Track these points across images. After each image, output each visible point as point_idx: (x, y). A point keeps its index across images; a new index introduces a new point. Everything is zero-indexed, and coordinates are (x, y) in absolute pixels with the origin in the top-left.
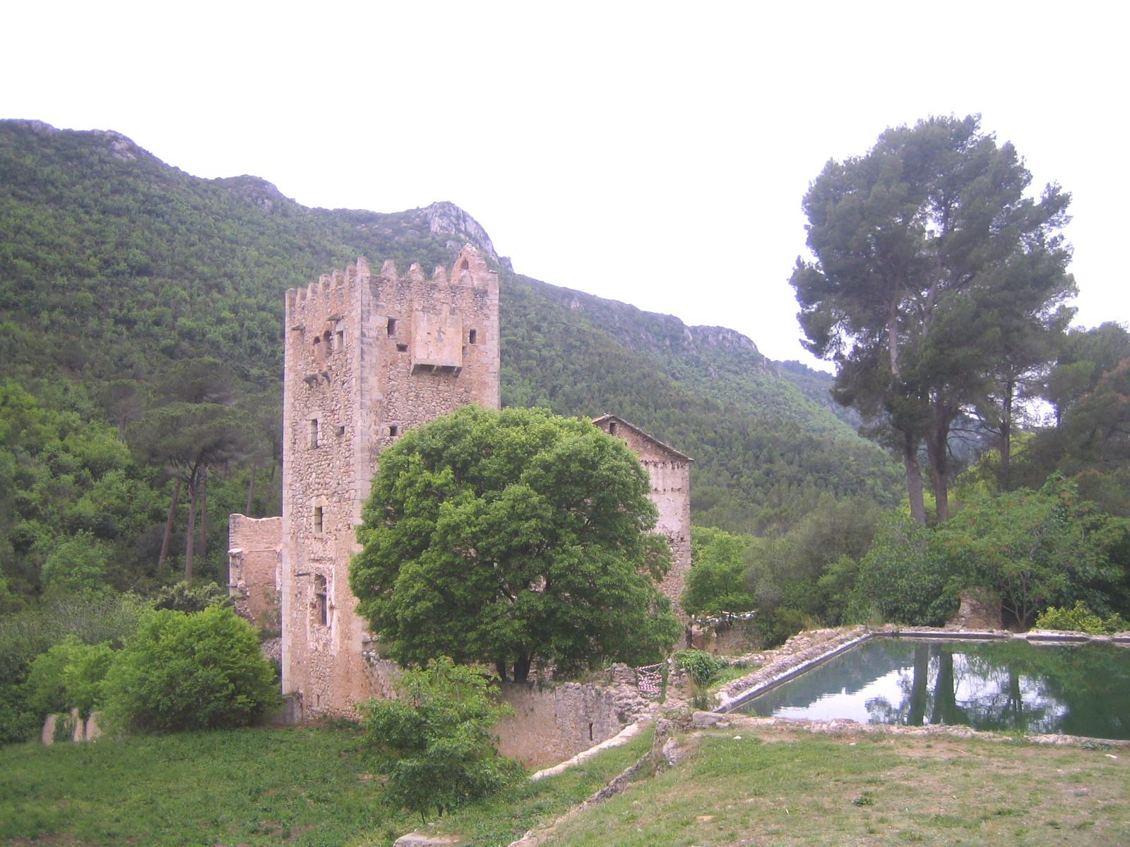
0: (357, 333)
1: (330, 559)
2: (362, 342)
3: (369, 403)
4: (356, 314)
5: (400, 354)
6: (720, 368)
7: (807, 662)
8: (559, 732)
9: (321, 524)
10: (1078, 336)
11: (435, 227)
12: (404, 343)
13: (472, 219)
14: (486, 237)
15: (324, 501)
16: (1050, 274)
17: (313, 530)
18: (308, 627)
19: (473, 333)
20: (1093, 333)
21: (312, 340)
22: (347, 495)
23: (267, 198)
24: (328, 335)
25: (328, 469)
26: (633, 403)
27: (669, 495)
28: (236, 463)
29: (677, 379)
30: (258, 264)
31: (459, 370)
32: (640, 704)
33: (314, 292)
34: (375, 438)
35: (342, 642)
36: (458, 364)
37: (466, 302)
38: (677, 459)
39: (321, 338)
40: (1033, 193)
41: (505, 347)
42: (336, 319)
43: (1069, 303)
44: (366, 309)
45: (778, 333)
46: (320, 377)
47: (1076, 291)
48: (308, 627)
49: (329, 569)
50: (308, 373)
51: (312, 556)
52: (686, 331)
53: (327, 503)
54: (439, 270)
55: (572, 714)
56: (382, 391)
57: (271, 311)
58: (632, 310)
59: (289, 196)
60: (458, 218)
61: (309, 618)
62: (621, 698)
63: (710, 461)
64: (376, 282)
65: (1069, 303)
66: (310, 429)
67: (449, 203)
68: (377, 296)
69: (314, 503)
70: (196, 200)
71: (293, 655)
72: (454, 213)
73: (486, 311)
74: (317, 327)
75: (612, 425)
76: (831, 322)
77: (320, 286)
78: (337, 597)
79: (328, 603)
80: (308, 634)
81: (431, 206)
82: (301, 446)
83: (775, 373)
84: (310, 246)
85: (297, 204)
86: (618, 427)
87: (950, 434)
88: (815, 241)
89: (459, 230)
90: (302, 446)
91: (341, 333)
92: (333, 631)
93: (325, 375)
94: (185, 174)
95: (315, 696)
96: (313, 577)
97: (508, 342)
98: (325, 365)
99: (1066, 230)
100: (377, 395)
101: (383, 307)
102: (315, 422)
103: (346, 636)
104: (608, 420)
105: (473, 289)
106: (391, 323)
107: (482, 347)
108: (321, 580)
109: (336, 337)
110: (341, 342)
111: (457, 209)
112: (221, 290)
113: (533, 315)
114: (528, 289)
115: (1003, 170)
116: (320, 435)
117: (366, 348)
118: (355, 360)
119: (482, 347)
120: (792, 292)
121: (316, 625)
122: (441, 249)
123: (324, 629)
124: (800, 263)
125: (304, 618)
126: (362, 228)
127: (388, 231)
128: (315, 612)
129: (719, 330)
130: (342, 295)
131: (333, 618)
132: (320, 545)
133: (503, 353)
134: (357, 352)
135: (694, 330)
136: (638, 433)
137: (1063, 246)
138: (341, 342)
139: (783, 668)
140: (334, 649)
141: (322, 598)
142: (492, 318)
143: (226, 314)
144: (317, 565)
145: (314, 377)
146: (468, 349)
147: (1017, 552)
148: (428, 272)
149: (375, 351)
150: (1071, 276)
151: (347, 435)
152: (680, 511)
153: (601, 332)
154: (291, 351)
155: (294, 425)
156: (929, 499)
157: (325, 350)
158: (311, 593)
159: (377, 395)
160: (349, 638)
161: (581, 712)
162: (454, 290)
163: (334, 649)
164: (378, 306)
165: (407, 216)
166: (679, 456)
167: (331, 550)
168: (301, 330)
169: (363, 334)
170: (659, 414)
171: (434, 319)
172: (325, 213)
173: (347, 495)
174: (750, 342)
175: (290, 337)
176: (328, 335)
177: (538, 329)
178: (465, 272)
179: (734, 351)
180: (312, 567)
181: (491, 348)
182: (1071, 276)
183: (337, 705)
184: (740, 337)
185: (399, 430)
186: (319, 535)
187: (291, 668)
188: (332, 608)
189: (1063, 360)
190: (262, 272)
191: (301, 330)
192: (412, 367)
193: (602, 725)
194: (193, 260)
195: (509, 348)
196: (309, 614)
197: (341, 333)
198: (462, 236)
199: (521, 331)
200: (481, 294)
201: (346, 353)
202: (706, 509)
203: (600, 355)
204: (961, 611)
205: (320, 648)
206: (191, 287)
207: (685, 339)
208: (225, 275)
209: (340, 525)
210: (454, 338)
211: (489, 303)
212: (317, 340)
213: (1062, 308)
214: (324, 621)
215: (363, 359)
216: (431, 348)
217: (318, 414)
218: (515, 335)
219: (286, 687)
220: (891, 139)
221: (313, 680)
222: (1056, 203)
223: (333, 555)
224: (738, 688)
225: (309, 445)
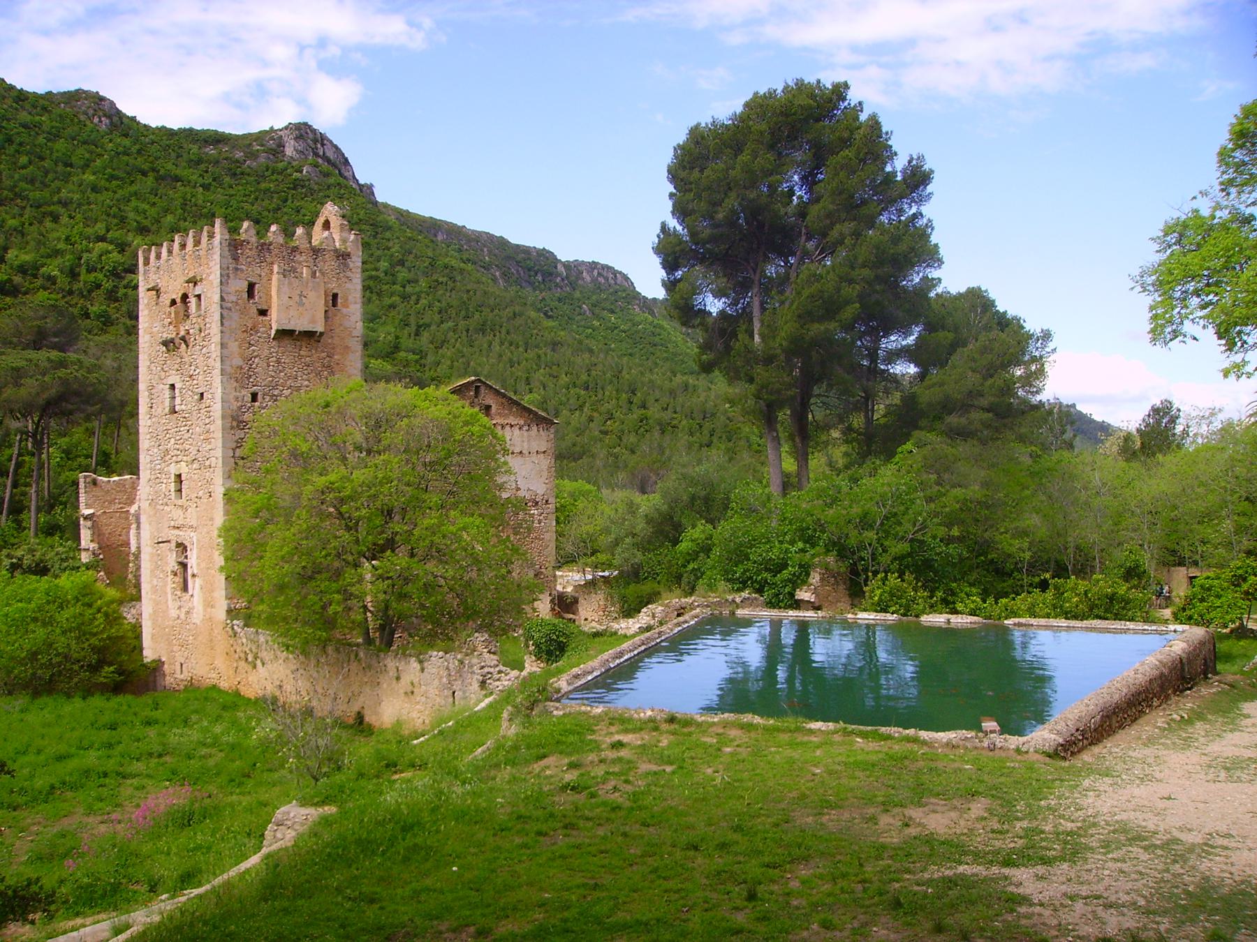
0: (217, 298)
1: (191, 527)
2: (222, 307)
3: (229, 369)
4: (215, 277)
5: (261, 318)
6: (594, 305)
7: (643, 648)
8: (423, 699)
9: (180, 490)
10: (944, 298)
11: (289, 151)
12: (265, 307)
13: (331, 142)
14: (346, 162)
15: (183, 469)
16: (916, 247)
17: (173, 496)
18: (169, 596)
19: (335, 296)
20: (960, 296)
21: (168, 302)
22: (207, 463)
23: (105, 115)
24: (185, 297)
25: (186, 436)
26: (502, 343)
27: (534, 458)
28: (82, 415)
29: (549, 317)
30: (95, 189)
31: (322, 334)
32: (500, 672)
33: (170, 252)
34: (235, 405)
35: (205, 610)
36: (320, 328)
37: (329, 264)
38: (543, 422)
39: (178, 300)
40: (899, 164)
41: (367, 283)
42: (194, 281)
43: (934, 274)
44: (225, 273)
45: (649, 280)
46: (177, 341)
47: (940, 262)
48: (169, 596)
49: (187, 536)
50: (165, 335)
51: (172, 523)
52: (559, 266)
53: (186, 470)
54: (300, 231)
55: (436, 682)
56: (242, 356)
57: (111, 243)
58: (502, 243)
59: (130, 114)
60: (315, 141)
61: (170, 586)
62: (482, 667)
63: (581, 407)
64: (234, 246)
65: (934, 274)
66: (167, 393)
67: (306, 124)
68: (236, 259)
69: (173, 470)
70: (24, 116)
71: (154, 621)
72: (311, 136)
73: (349, 274)
74: (174, 289)
75: (477, 387)
76: (695, 291)
77: (176, 246)
78: (198, 564)
79: (190, 572)
80: (170, 602)
81: (286, 128)
82: (158, 410)
83: (652, 313)
84: (153, 170)
85: (139, 123)
86: (483, 389)
87: (812, 400)
88: (680, 211)
89: (316, 154)
90: (160, 410)
91: (199, 296)
92: (195, 598)
93: (183, 339)
94: (12, 87)
95: (178, 665)
96: (173, 544)
97: (371, 277)
98: (182, 328)
99: (925, 209)
100: (238, 361)
101: (242, 270)
102: (173, 387)
103: (209, 604)
104: (473, 382)
105: (336, 250)
106: (251, 287)
107: (344, 310)
108: (182, 547)
109: (193, 300)
110: (199, 305)
111: (314, 131)
112: (56, 218)
113: (397, 247)
114: (392, 219)
115: (871, 142)
116: (178, 401)
117: (225, 313)
118: (214, 325)
119: (344, 310)
120: (656, 261)
121: (179, 593)
122: (298, 175)
123: (187, 597)
124: (664, 227)
125: (165, 586)
126: (211, 151)
127: (239, 155)
128: (177, 579)
129: (593, 265)
130: (199, 257)
131: (195, 586)
132: (180, 512)
133: (366, 288)
134: (217, 317)
135: (567, 265)
136: (504, 396)
137: (921, 222)
138: (199, 305)
139: (621, 654)
140: (197, 617)
141: (184, 566)
142: (355, 281)
143: (61, 246)
144: (177, 532)
145: (172, 341)
146: (330, 314)
147: (865, 523)
148: (288, 233)
149: (235, 316)
150: (936, 245)
151: (206, 401)
152: (545, 474)
153: (470, 267)
154: (146, 312)
155: (151, 388)
156: (789, 465)
157: (182, 314)
158: (172, 561)
159: (238, 361)
160: (212, 607)
161: (445, 680)
162: (316, 252)
163: (197, 617)
164: (237, 269)
165: (261, 137)
166: (544, 418)
167: (192, 517)
168: (156, 290)
169: (222, 299)
170: (531, 354)
171: (296, 282)
172: (170, 133)
173: (207, 463)
174: (626, 278)
175: (144, 297)
176: (185, 297)
177: (402, 263)
178: (326, 233)
179: (608, 286)
180: (173, 535)
181: (354, 312)
182: (936, 245)
183: (201, 673)
184: (616, 273)
185: (259, 397)
186: (179, 502)
187: (153, 635)
188: (194, 576)
189: (931, 328)
190: (100, 198)
191: (156, 290)
192: (273, 332)
193: (464, 692)
194: (23, 185)
195: (371, 283)
196: (171, 583)
197: (199, 296)
198: (320, 161)
199: (384, 265)
200: (343, 256)
201: (205, 317)
202: (575, 460)
203: (468, 291)
204: (811, 580)
205: (183, 616)
206: (21, 215)
207: (559, 275)
208: (60, 202)
209: (201, 493)
210: (318, 303)
211: (351, 265)
212: (173, 302)
213: (925, 278)
214: (185, 588)
215: (222, 324)
216: (292, 313)
217: (174, 379)
218: (377, 270)
219: (149, 654)
220: (759, 106)
221: (175, 648)
222: (918, 179)
223: (194, 523)
224: (577, 677)
225: (167, 410)
